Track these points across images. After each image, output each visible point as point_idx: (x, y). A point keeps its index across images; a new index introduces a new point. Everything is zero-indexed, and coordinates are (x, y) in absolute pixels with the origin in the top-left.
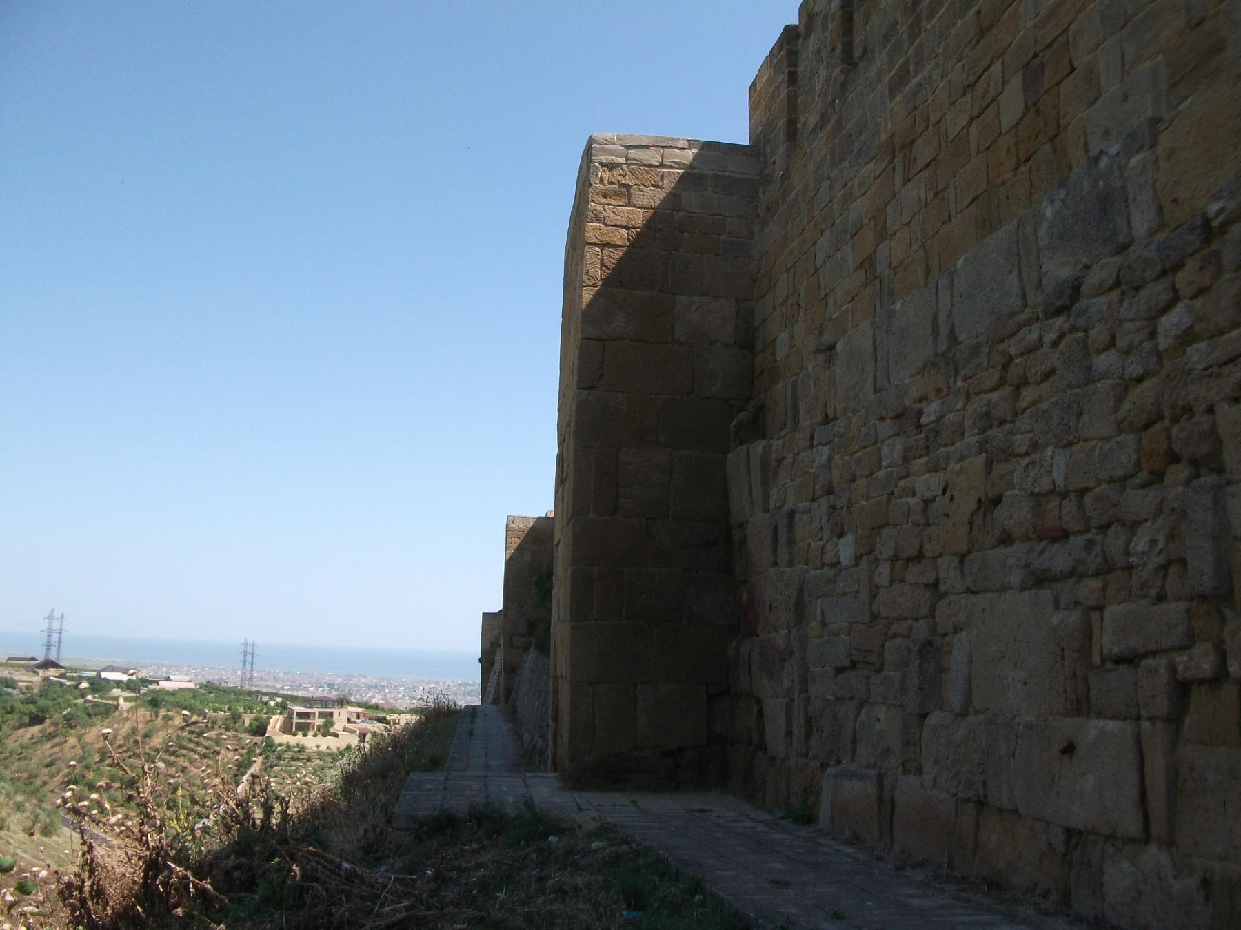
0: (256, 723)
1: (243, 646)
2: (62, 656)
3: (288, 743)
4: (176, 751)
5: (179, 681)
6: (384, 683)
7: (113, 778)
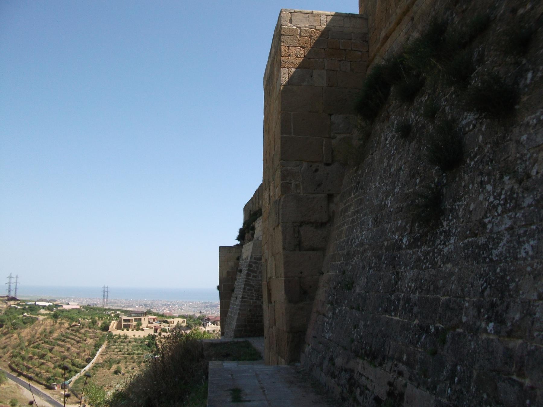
0: (104, 325)
1: (103, 288)
2: (18, 294)
3: (119, 334)
4: (65, 340)
5: (73, 305)
6: (169, 303)
7: (34, 354)
